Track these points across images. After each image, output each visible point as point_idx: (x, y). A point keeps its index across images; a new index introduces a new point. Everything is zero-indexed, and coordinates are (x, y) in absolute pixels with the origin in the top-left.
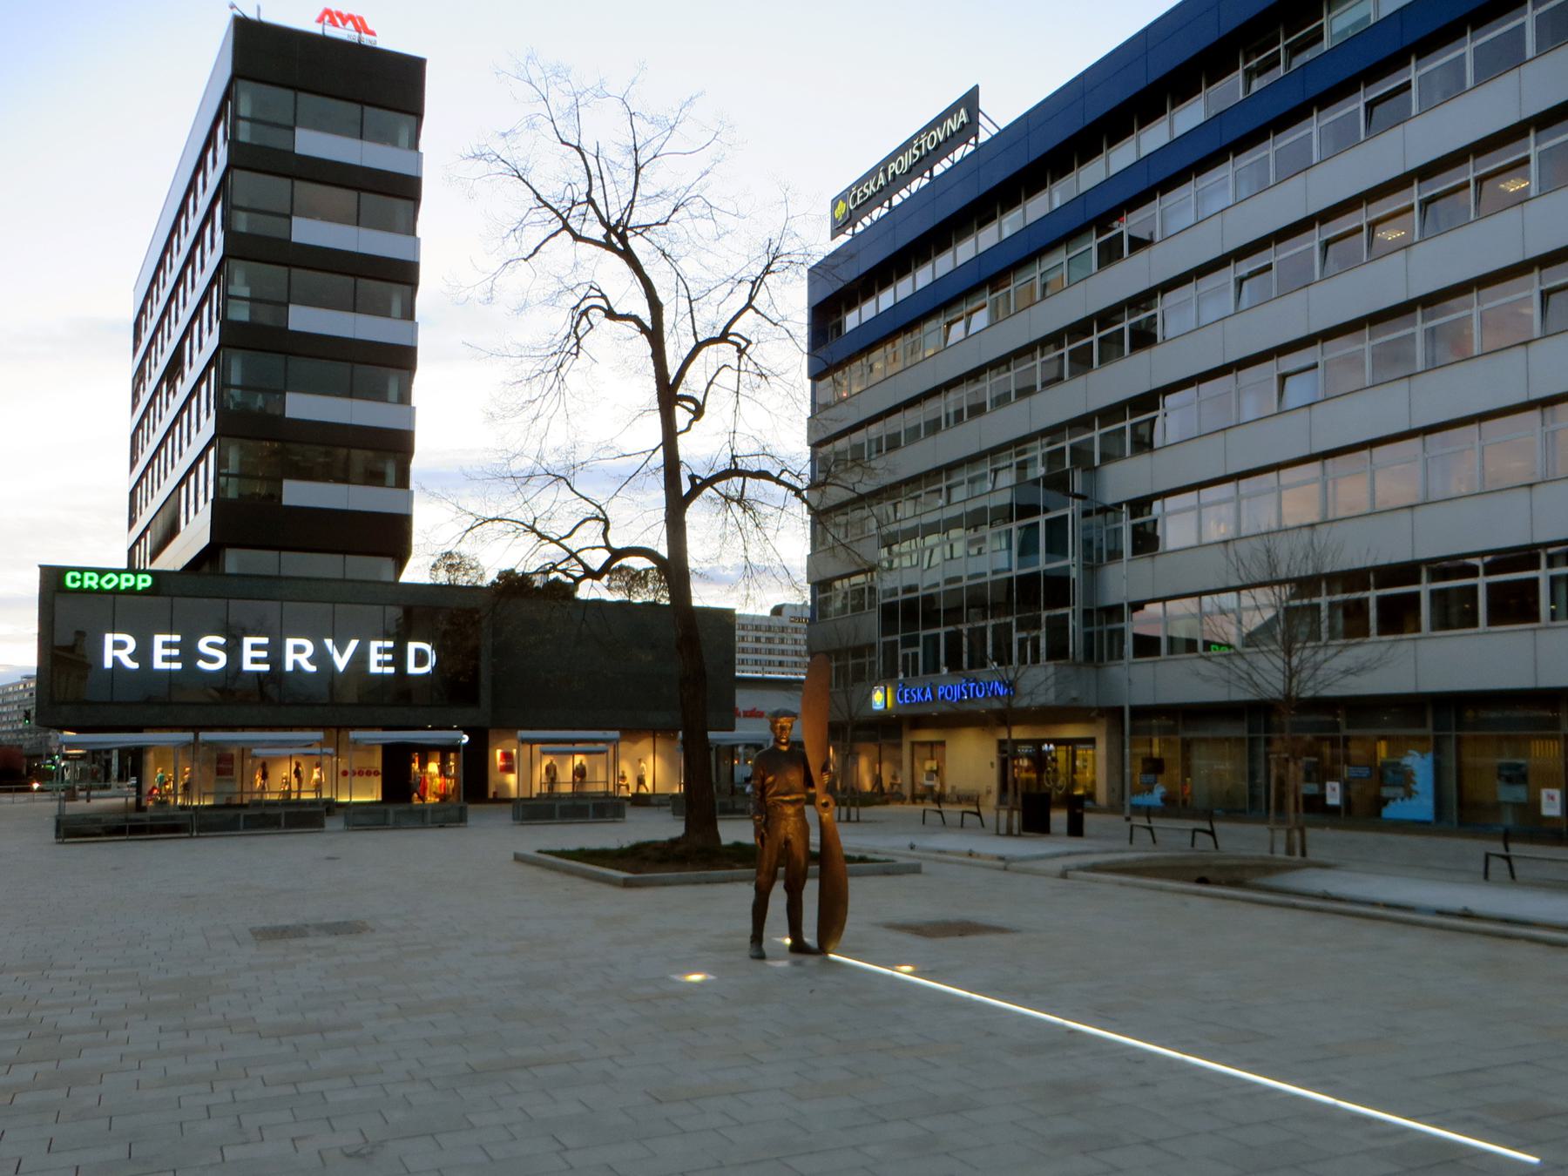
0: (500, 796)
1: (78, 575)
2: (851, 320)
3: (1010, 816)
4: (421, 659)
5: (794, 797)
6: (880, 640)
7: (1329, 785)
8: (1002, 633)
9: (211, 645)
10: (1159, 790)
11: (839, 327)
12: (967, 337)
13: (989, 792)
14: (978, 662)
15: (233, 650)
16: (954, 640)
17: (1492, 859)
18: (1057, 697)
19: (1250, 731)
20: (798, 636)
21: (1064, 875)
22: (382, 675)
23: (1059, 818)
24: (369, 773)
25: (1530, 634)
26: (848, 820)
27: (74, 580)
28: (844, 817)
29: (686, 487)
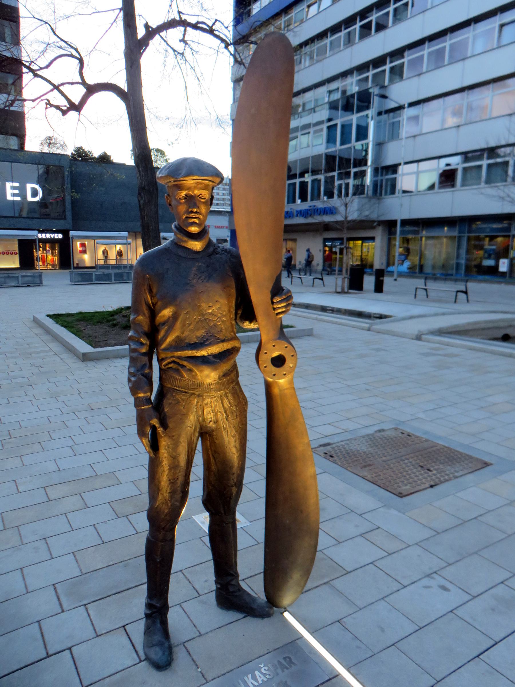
0: (80, 265)
3: (343, 282)
4: (35, 193)
5: (215, 349)
8: (330, 181)
10: (407, 264)
11: (249, 13)
12: (319, 13)
14: (316, 196)
16: (304, 185)
18: (359, 216)
19: (460, 232)
20: (225, 319)
21: (419, 338)
22: (14, 202)
23: (369, 281)
24: (12, 253)
25: (451, 193)
29: (141, 32)
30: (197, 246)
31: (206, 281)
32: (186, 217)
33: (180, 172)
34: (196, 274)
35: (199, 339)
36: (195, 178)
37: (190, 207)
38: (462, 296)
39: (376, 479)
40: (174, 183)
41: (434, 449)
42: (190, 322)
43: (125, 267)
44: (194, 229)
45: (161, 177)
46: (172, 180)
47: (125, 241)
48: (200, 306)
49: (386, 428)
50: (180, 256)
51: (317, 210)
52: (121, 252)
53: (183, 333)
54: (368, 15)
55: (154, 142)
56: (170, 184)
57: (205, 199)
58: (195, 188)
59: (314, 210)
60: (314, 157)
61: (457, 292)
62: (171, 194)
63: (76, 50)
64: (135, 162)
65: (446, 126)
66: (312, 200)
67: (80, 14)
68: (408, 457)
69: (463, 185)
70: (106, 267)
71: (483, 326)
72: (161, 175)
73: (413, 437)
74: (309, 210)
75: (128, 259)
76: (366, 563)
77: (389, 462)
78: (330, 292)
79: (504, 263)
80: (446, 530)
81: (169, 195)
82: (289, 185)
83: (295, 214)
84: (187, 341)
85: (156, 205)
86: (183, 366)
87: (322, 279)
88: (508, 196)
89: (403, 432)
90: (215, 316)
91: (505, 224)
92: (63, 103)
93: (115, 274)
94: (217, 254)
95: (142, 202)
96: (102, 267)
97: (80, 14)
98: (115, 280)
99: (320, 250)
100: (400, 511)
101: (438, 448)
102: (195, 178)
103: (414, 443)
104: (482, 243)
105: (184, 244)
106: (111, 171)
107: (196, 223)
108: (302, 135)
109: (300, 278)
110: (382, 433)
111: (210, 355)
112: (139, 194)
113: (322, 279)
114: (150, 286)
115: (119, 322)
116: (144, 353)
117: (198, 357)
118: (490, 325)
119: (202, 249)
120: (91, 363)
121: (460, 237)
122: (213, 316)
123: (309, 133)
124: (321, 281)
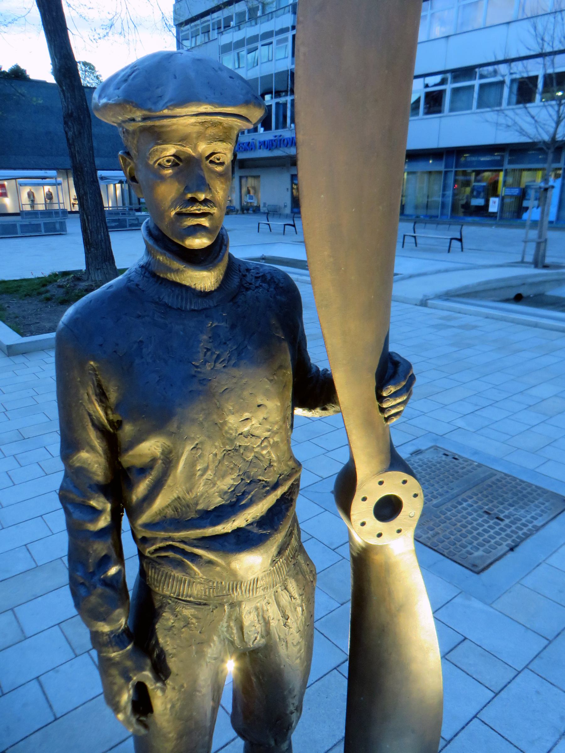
7: (492, 200)
13: (285, 206)
17: (406, 237)
19: (446, 167)
21: (424, 303)
25: (438, 120)
30: (205, 280)
31: (234, 365)
32: (179, 214)
33: (159, 91)
34: (208, 350)
35: (226, 497)
36: (203, 108)
37: (187, 189)
38: (456, 244)
39: (435, 540)
40: (141, 124)
41: (493, 479)
42: (206, 465)
43: (57, 212)
44: (199, 242)
45: (106, 105)
46: (138, 114)
47: (53, 181)
48: (225, 423)
49: (423, 448)
50: (166, 306)
51: (284, 140)
52: (51, 194)
53: (189, 491)
55: (81, 51)
56: (131, 127)
57: (222, 164)
58: (201, 136)
59: (280, 140)
60: (278, 74)
61: (452, 239)
62: (133, 152)
64: (56, 79)
65: (433, 37)
66: (277, 128)
68: (464, 496)
69: (452, 110)
70: (34, 214)
71: (494, 285)
72: (104, 101)
73: (461, 461)
75: (59, 203)
76: (469, 719)
77: (443, 508)
79: (495, 202)
80: (558, 635)
81: (128, 154)
83: (258, 145)
84: (200, 507)
85: (90, 136)
86: (194, 557)
88: (515, 123)
89: (447, 453)
90: (258, 437)
91: (497, 157)
93: (45, 224)
94: (247, 289)
95: (70, 134)
96: (28, 213)
98: (45, 232)
99: (288, 189)
100: (486, 603)
101: (498, 477)
102: (203, 108)
103: (465, 470)
104: (468, 178)
105: (177, 278)
106: (23, 90)
107: (204, 227)
108: (262, 45)
109: (269, 224)
110: (420, 456)
111: (251, 524)
112: (66, 123)
114: (100, 386)
115: (54, 295)
116: (103, 530)
117: (227, 534)
118: (502, 284)
119: (217, 285)
120: (20, 359)
121: (446, 172)
122: (253, 439)
123: (271, 43)
124: (293, 228)
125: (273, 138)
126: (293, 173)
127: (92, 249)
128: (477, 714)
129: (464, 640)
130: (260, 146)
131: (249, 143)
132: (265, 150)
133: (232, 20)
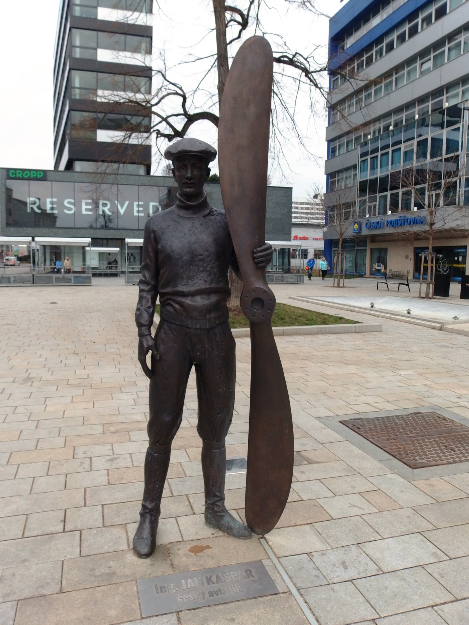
1: (14, 172)
2: (349, 42)
3: (428, 287)
6: (358, 200)
9: (69, 203)
13: (408, 273)
15: (77, 204)
16: (395, 198)
26: (339, 286)
27: (13, 174)
28: (336, 285)
51: (407, 220)
54: (455, 38)
59: (404, 220)
63: (181, 89)
67: (186, 62)
74: (400, 220)
78: (416, 297)
82: (380, 197)
87: (408, 285)
92: (169, 131)
97: (186, 62)
109: (387, 283)
113: (408, 285)
123: (430, 59)
125: (398, 218)
126: (416, 246)
127: (235, 283)
128: (453, 601)
129: (48, 474)
130: (388, 225)
131: (379, 222)
132: (392, 228)
133: (391, 125)
